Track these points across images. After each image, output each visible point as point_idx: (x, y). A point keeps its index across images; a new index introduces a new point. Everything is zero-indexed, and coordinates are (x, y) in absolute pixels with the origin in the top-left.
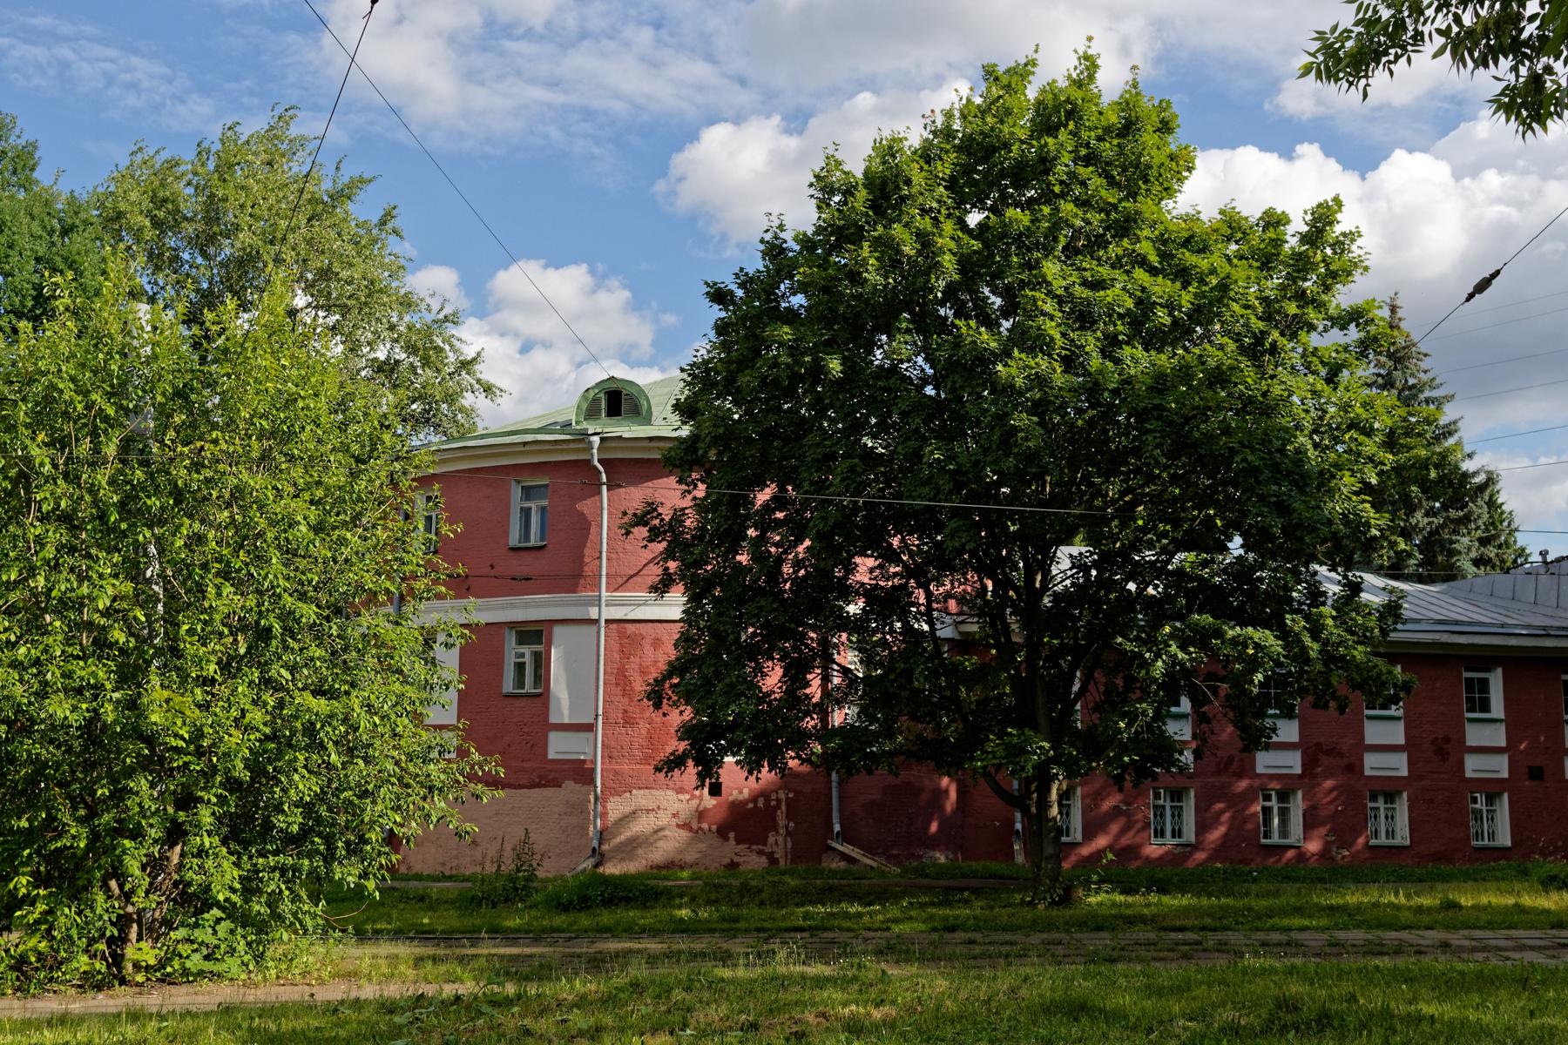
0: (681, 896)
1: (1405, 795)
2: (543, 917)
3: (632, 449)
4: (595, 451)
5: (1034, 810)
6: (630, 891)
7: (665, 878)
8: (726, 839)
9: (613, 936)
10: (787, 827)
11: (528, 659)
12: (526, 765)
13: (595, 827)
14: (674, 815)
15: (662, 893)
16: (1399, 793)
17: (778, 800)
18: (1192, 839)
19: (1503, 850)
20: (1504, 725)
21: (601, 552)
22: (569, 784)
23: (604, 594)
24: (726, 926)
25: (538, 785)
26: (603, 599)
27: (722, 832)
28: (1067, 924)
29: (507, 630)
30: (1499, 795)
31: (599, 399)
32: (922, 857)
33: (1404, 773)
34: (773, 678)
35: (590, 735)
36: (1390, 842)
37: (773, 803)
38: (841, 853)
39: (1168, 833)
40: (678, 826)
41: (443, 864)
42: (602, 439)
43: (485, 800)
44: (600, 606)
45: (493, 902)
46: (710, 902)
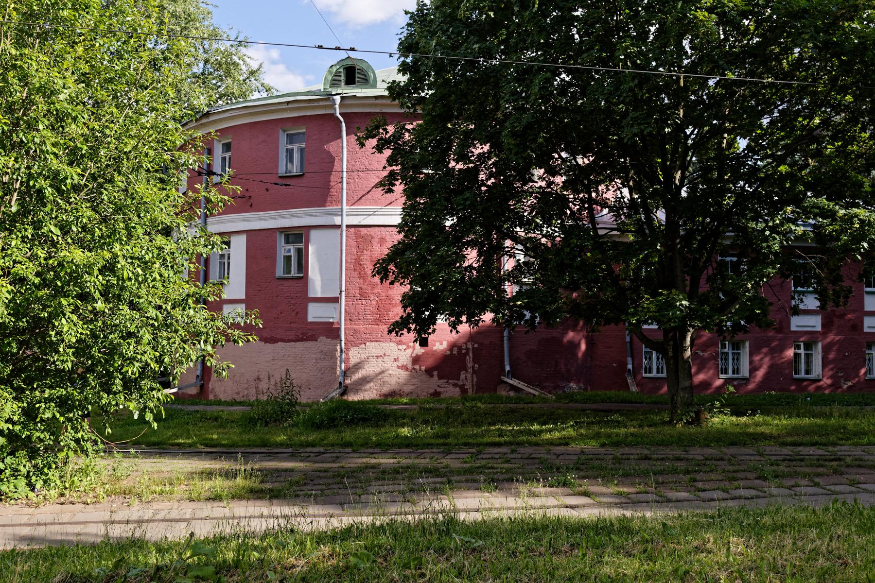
0: (404, 418)
2: (301, 434)
3: (363, 105)
4: (337, 106)
6: (366, 414)
7: (390, 403)
9: (354, 451)
10: (473, 367)
11: (293, 253)
12: (294, 325)
13: (340, 368)
14: (396, 360)
15: (389, 416)
17: (467, 349)
18: (747, 375)
21: (342, 178)
22: (322, 339)
23: (345, 207)
24: (441, 441)
25: (301, 340)
26: (344, 211)
27: (429, 372)
28: (705, 439)
29: (278, 234)
31: (340, 73)
32: (564, 387)
33: (819, 328)
34: (472, 256)
35: (337, 305)
37: (464, 351)
38: (511, 385)
39: (730, 371)
40: (398, 367)
41: (238, 393)
42: (342, 98)
43: (241, 344)
44: (342, 216)
45: (266, 422)
46: (426, 422)
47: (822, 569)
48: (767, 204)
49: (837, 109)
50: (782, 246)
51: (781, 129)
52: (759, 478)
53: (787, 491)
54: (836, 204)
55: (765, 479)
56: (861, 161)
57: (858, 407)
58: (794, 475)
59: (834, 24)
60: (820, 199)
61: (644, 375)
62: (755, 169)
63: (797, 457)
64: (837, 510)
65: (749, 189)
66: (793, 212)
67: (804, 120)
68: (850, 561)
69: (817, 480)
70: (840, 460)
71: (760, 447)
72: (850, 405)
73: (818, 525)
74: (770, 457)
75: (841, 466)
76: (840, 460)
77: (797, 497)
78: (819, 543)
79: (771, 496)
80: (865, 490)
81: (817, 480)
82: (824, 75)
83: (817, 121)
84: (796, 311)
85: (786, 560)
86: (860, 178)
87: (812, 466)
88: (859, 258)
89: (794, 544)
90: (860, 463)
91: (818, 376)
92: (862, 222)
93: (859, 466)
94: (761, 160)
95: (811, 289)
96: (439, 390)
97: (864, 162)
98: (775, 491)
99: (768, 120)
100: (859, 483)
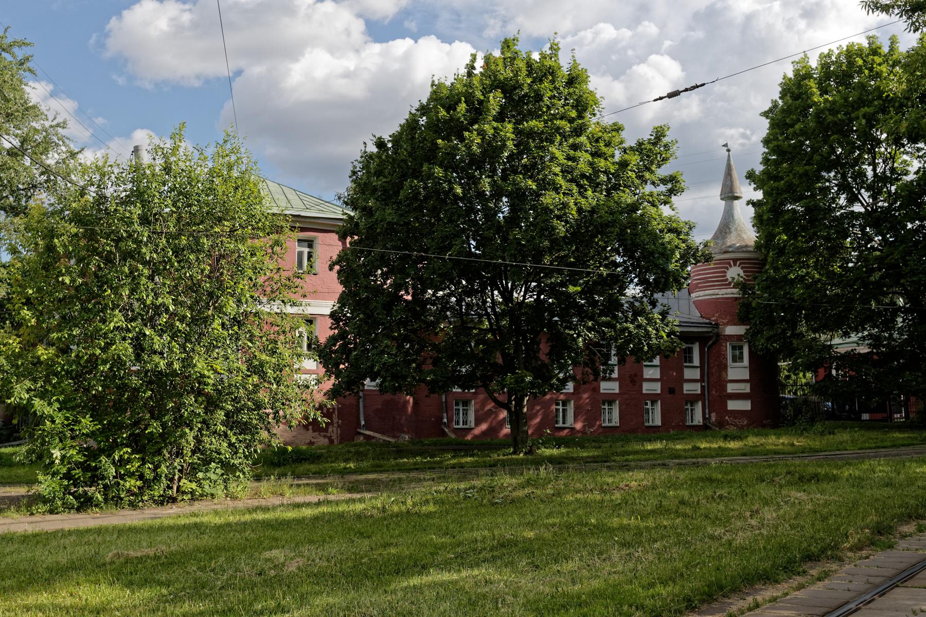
1: (617, 402)
5: (513, 409)
8: (308, 430)
16: (614, 401)
19: (658, 427)
20: (699, 369)
30: (656, 401)
33: (617, 391)
36: (610, 425)
61: (455, 427)
96: (313, 440)
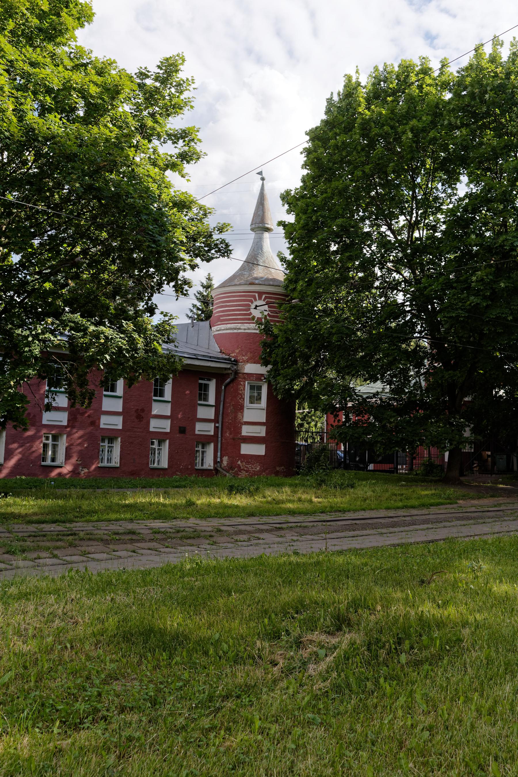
33: (65, 423)
47: (58, 629)
48: (31, 313)
49: (96, 241)
50: (41, 352)
51: (49, 251)
52: (7, 553)
53: (31, 563)
54: (88, 321)
55: (13, 553)
56: (110, 288)
57: (91, 490)
58: (38, 548)
59: (96, 173)
60: (76, 315)
62: (24, 283)
63: (40, 533)
64: (71, 578)
65: (17, 299)
66: (53, 324)
67: (68, 246)
68: (80, 620)
69: (56, 552)
70: (75, 534)
71: (10, 526)
72: (85, 488)
73: (57, 591)
74: (18, 534)
75: (75, 540)
76: (75, 534)
77: (40, 568)
78: (56, 607)
79: (18, 568)
80: (93, 559)
81: (56, 552)
82: (87, 212)
83: (78, 249)
84: (49, 408)
85: (28, 624)
86: (108, 302)
87: (52, 540)
88: (102, 367)
89: (36, 609)
90: (91, 536)
91: (62, 463)
92: (106, 338)
93: (90, 539)
94: (30, 275)
95: (63, 390)
97: (111, 289)
98: (21, 563)
99: (39, 241)
100: (89, 553)
